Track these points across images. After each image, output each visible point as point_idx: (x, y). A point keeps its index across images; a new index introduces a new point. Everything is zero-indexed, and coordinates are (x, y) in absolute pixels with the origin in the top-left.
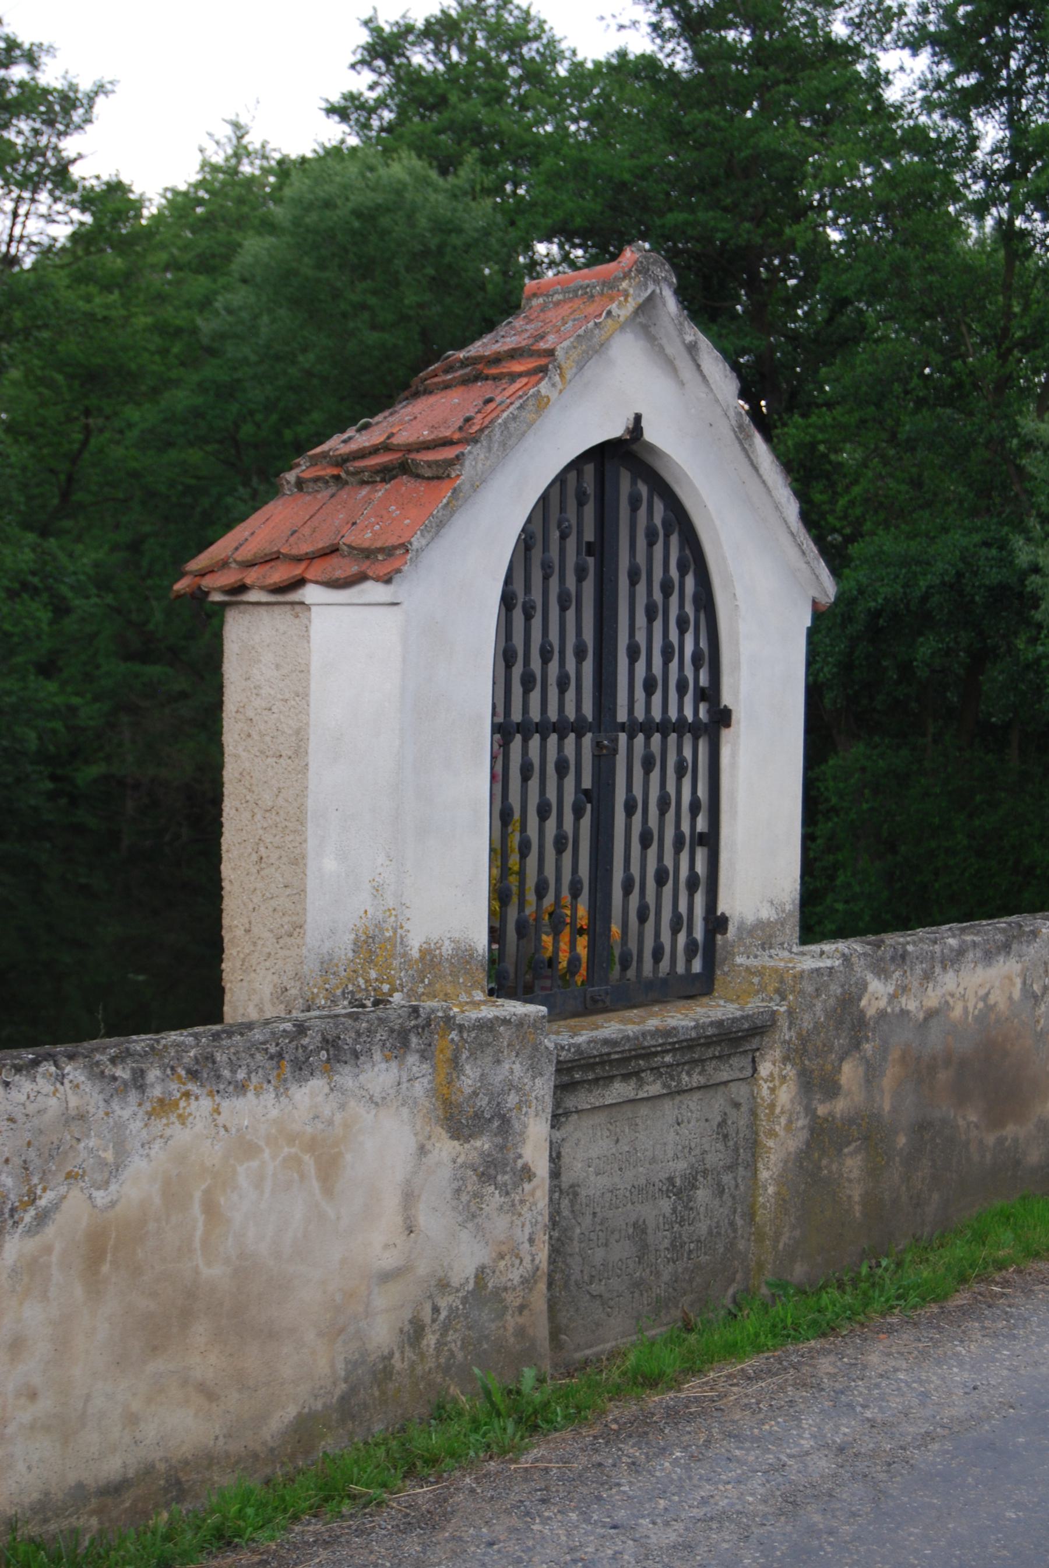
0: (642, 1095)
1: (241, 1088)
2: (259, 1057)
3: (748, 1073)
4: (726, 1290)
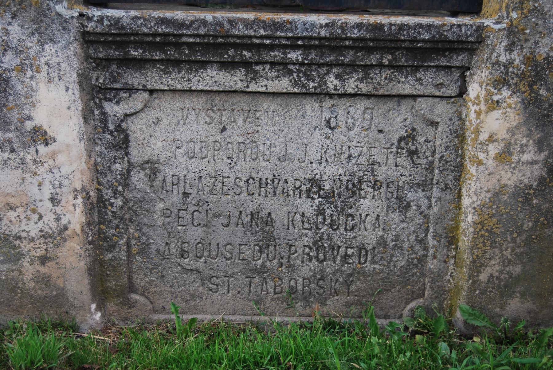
0: (253, 87)
3: (453, 90)
4: (407, 303)
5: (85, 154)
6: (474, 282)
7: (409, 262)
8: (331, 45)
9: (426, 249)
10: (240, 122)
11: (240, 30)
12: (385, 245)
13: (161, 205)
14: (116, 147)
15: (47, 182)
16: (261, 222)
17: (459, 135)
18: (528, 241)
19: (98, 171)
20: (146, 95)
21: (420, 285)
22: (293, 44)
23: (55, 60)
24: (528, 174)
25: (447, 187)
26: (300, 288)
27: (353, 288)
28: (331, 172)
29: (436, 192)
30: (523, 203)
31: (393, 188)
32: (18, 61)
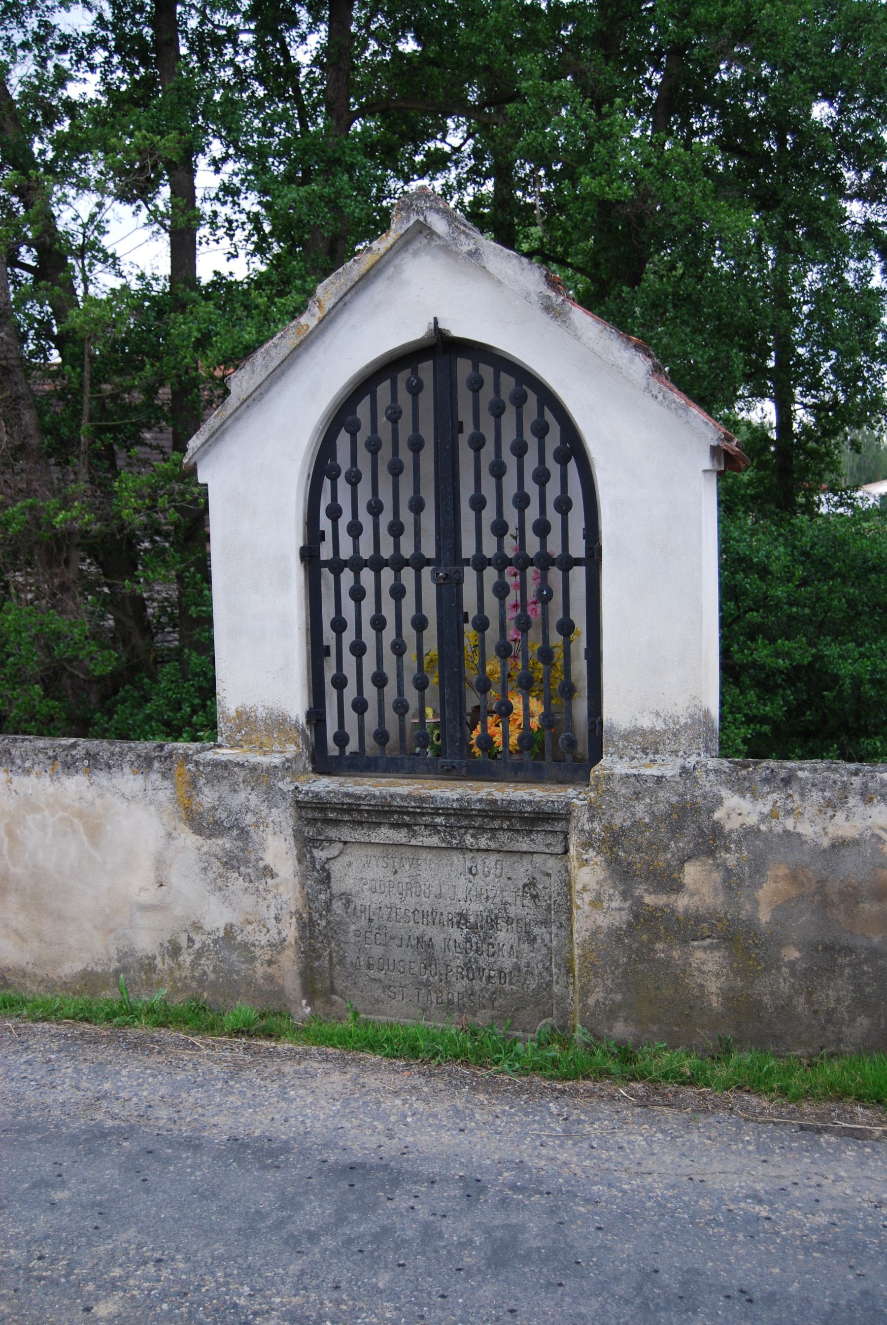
0: (413, 842)
1: (27, 772)
2: (41, 756)
3: (559, 849)
4: (540, 1021)
5: (298, 886)
6: (584, 1005)
7: (540, 986)
8: (462, 816)
9: (551, 975)
10: (407, 867)
11: (398, 802)
12: (519, 970)
13: (353, 927)
14: (321, 882)
15: (272, 906)
16: (424, 945)
17: (568, 884)
18: (625, 974)
19: (309, 900)
20: (341, 845)
21: (549, 1005)
22: (436, 812)
23: (278, 819)
24: (618, 918)
25: (561, 925)
26: (456, 1000)
27: (496, 1004)
28: (474, 908)
29: (554, 929)
30: (617, 942)
31: (521, 924)
32: (255, 819)
